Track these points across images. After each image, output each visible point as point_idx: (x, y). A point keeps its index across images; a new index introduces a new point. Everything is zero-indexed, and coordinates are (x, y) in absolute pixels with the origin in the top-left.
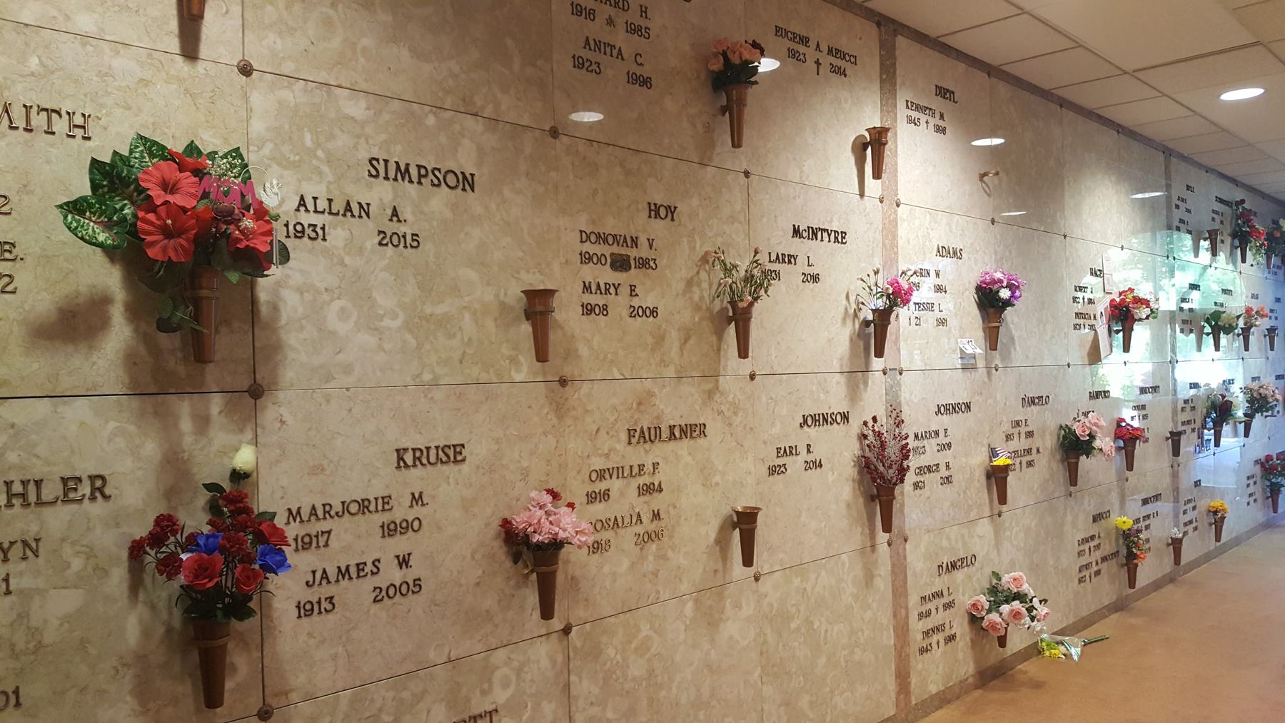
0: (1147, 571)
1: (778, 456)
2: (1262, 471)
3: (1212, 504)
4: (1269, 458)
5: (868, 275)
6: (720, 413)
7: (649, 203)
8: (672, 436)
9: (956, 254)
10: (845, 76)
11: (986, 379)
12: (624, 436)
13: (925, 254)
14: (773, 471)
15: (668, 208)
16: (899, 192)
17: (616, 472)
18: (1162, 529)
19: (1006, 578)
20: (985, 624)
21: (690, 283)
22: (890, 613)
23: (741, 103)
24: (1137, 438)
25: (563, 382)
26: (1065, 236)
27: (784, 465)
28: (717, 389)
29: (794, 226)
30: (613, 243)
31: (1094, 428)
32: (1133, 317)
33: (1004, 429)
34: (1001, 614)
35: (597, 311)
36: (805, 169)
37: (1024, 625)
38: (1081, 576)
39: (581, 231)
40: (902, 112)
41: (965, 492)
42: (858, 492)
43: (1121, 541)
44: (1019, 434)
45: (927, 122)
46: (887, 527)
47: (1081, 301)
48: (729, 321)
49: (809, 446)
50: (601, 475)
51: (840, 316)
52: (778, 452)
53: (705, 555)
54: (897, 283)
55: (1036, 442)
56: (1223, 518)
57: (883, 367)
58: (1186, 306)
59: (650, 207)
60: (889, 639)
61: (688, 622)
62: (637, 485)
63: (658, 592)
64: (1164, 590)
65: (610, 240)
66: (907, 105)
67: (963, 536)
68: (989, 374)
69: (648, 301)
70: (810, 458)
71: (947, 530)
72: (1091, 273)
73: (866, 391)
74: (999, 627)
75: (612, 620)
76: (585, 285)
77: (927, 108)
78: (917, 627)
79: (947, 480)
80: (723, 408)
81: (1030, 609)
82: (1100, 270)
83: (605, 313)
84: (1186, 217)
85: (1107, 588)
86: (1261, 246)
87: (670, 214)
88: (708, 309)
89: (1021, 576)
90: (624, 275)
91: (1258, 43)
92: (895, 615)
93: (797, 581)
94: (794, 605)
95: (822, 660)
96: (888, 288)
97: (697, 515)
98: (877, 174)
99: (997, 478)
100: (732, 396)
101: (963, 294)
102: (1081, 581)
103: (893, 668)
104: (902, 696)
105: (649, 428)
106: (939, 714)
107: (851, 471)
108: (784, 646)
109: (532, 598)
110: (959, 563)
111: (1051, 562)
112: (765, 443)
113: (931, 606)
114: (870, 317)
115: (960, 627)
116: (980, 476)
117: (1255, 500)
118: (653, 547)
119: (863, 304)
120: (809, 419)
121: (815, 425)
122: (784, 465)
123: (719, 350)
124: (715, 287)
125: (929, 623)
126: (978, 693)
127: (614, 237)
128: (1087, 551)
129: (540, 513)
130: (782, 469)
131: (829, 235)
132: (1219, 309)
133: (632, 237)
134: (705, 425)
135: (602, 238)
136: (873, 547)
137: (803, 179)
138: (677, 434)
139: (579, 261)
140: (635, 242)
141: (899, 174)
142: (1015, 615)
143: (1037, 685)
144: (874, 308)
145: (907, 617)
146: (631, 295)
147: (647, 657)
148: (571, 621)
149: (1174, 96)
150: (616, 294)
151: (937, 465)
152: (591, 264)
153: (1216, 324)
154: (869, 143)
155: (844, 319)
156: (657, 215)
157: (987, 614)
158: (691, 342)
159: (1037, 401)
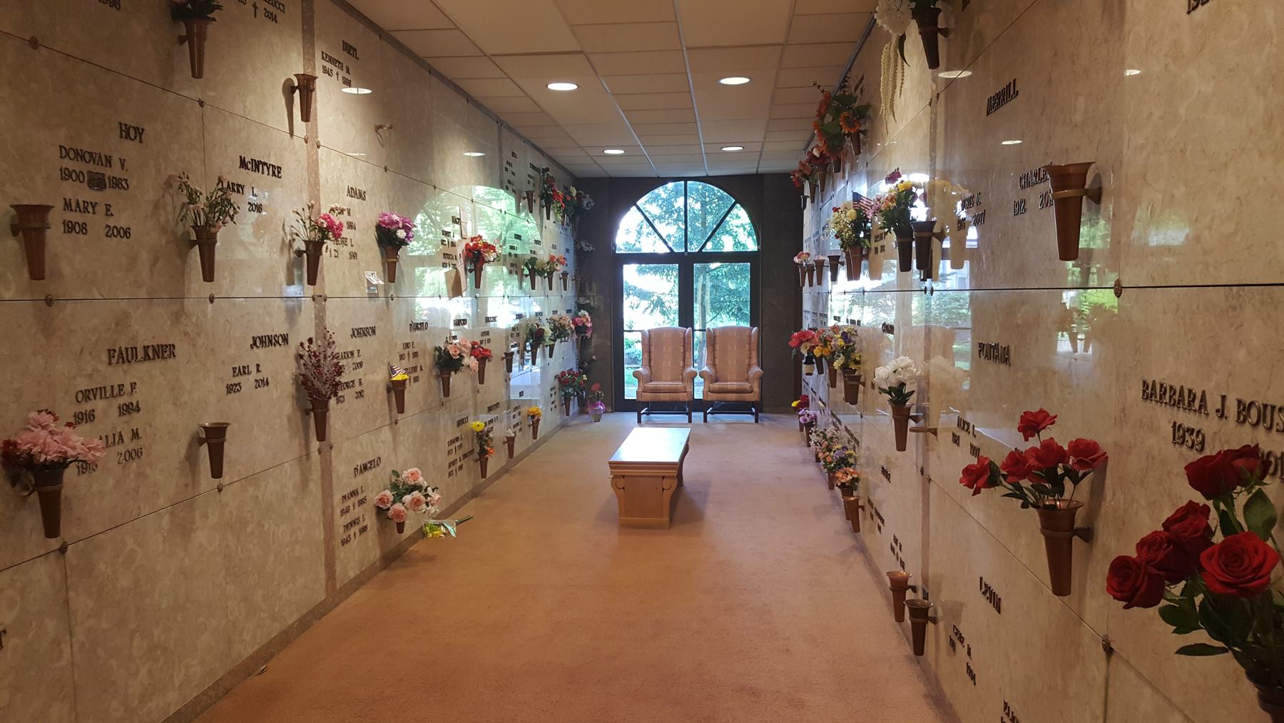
0: (493, 465)
1: (234, 376)
2: (559, 384)
3: (530, 410)
4: (563, 373)
5: (303, 209)
6: (186, 334)
7: (120, 123)
8: (147, 357)
9: (361, 196)
10: (276, 22)
11: (385, 307)
12: (105, 357)
13: (339, 193)
14: (232, 389)
15: (136, 129)
16: (319, 135)
17: (98, 393)
18: (500, 431)
19: (405, 474)
20: (390, 513)
21: (157, 206)
22: (320, 512)
23: (202, 37)
24: (487, 357)
25: (49, 301)
26: (435, 188)
27: (239, 384)
28: (183, 310)
29: (241, 157)
30: (90, 161)
31: (463, 349)
32: (484, 259)
33: (398, 350)
34: (403, 504)
35: (77, 230)
36: (247, 104)
37: (421, 510)
38: (450, 470)
39: (61, 147)
40: (320, 63)
41: (372, 405)
42: (296, 407)
43: (475, 441)
44: (409, 354)
45: (337, 74)
46: (321, 436)
47: (447, 243)
48: (192, 244)
49: (258, 365)
50: (87, 395)
51: (279, 245)
52: (234, 372)
53: (178, 471)
54: (329, 218)
55: (420, 361)
56: (538, 420)
57: (312, 294)
58: (513, 252)
59: (121, 127)
60: (320, 535)
61: (166, 534)
62: (118, 405)
63: (139, 508)
64: (502, 479)
65: (87, 156)
66: (323, 57)
67: (371, 442)
68: (387, 303)
69: (122, 221)
70: (259, 377)
71: (361, 437)
72: (453, 220)
73: (300, 315)
74: (403, 514)
75: (102, 536)
76: (66, 203)
77: (337, 61)
78: (340, 521)
79: (360, 394)
80: (189, 329)
81: (426, 496)
82: (458, 219)
83: (84, 231)
84: (512, 178)
85: (465, 482)
86: (560, 207)
87: (138, 136)
88: (173, 231)
89: (417, 471)
90: (100, 194)
91: (581, 52)
92: (324, 513)
93: (251, 490)
94: (249, 511)
95: (272, 558)
96: (322, 223)
97: (169, 432)
98: (306, 117)
99: (396, 390)
100: (195, 318)
101: (367, 231)
102: (450, 474)
103: (323, 559)
104: (330, 583)
105: (126, 349)
106: (357, 594)
107: (290, 388)
108: (242, 548)
109: (32, 520)
110: (369, 465)
111: (431, 460)
112: (223, 362)
113: (350, 503)
114: (303, 248)
115: (370, 520)
116: (382, 389)
117: (555, 407)
118: (134, 465)
119: (297, 235)
120: (258, 340)
121: (263, 346)
122: (239, 384)
123: (183, 273)
124: (178, 210)
125: (348, 518)
126: (384, 573)
127: (91, 154)
128: (454, 450)
129: (44, 433)
130: (238, 387)
131: (268, 169)
132: (533, 256)
133: (106, 156)
134: (174, 346)
135: (80, 155)
136: (308, 455)
137: (247, 113)
138: (151, 354)
139: (60, 178)
140: (109, 161)
141: (318, 118)
142: (416, 502)
143: (430, 559)
144: (307, 239)
145: (333, 514)
146: (107, 215)
147: (133, 569)
148: (66, 540)
149: (513, 79)
150: (94, 213)
151: (353, 381)
152: (70, 181)
153: (533, 267)
154: (297, 87)
155: (282, 249)
156: (128, 137)
157: (392, 505)
158: (160, 264)
159: (419, 326)
